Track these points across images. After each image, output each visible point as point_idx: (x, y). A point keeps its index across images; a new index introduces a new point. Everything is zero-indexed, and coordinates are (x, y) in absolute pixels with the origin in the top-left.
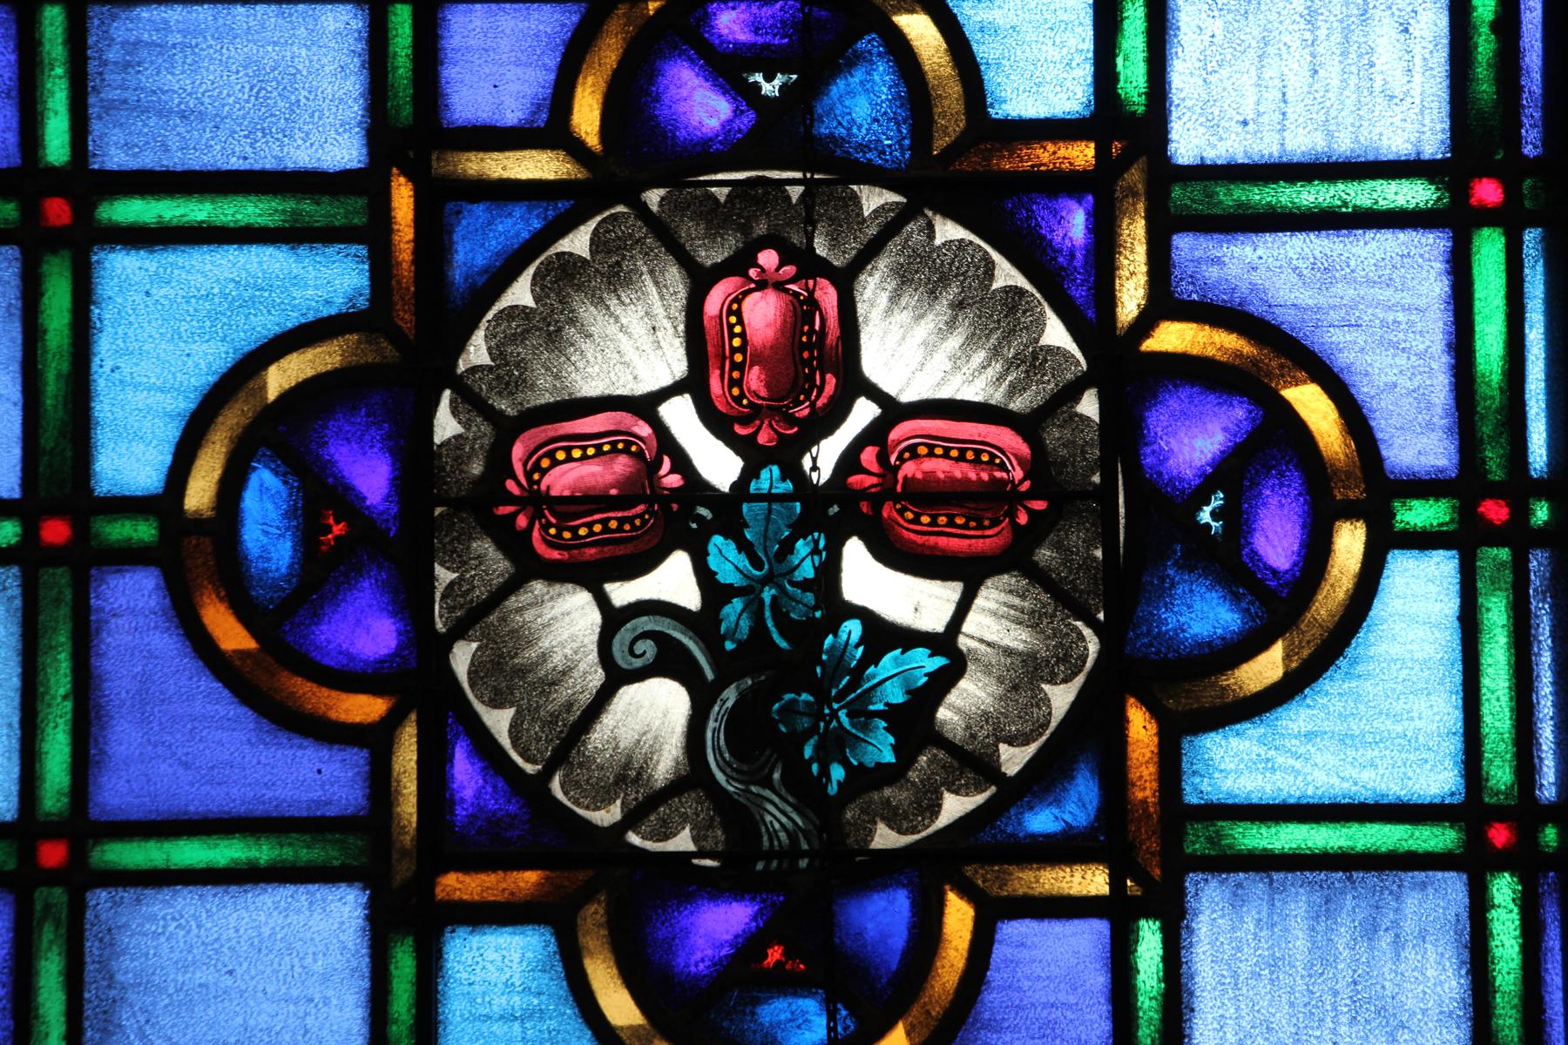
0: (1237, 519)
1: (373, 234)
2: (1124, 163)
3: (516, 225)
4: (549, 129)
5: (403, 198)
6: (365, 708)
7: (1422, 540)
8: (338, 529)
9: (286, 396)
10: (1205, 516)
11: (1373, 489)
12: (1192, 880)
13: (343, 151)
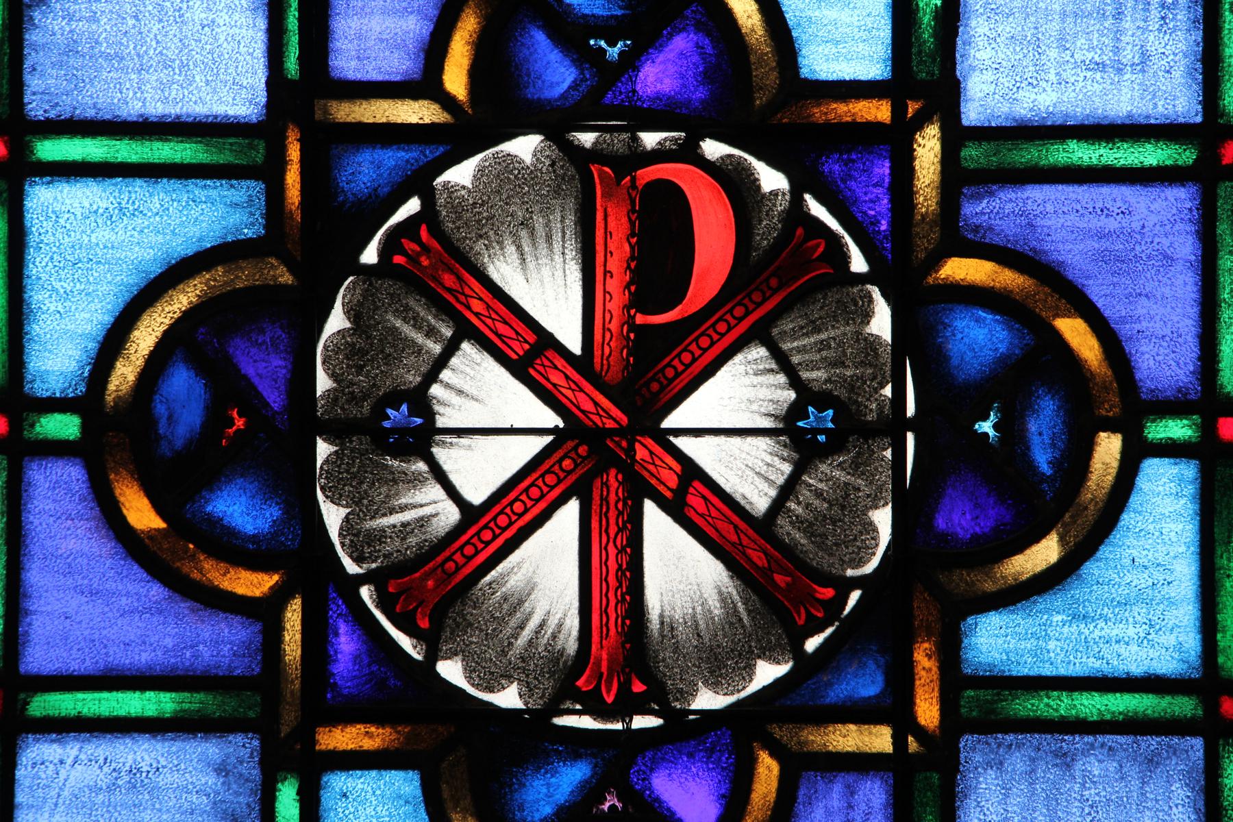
0: (215, 417)
1: (955, 678)
2: (919, 123)
3: (392, 159)
4: (426, 84)
5: (928, 712)
6: (253, 584)
7: (1171, 450)
8: (240, 423)
9: (1036, 537)
10: (240, 423)
11: (1133, 408)
12: (966, 741)
13: (973, 750)
